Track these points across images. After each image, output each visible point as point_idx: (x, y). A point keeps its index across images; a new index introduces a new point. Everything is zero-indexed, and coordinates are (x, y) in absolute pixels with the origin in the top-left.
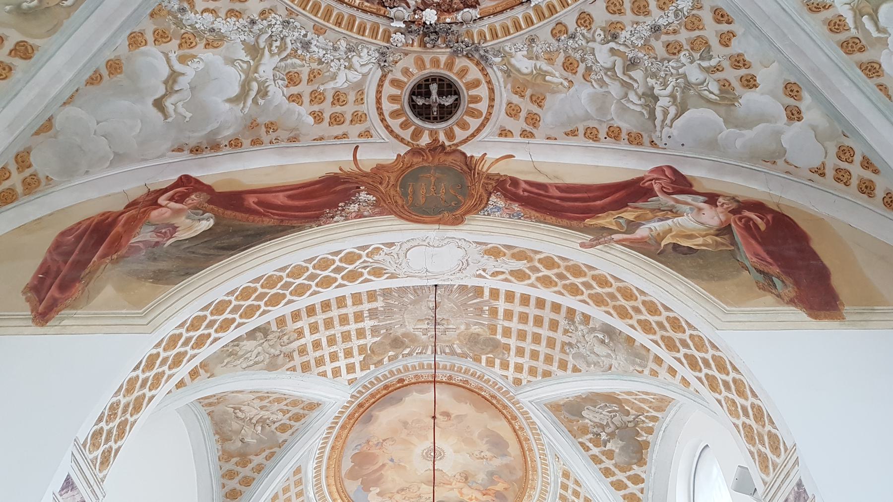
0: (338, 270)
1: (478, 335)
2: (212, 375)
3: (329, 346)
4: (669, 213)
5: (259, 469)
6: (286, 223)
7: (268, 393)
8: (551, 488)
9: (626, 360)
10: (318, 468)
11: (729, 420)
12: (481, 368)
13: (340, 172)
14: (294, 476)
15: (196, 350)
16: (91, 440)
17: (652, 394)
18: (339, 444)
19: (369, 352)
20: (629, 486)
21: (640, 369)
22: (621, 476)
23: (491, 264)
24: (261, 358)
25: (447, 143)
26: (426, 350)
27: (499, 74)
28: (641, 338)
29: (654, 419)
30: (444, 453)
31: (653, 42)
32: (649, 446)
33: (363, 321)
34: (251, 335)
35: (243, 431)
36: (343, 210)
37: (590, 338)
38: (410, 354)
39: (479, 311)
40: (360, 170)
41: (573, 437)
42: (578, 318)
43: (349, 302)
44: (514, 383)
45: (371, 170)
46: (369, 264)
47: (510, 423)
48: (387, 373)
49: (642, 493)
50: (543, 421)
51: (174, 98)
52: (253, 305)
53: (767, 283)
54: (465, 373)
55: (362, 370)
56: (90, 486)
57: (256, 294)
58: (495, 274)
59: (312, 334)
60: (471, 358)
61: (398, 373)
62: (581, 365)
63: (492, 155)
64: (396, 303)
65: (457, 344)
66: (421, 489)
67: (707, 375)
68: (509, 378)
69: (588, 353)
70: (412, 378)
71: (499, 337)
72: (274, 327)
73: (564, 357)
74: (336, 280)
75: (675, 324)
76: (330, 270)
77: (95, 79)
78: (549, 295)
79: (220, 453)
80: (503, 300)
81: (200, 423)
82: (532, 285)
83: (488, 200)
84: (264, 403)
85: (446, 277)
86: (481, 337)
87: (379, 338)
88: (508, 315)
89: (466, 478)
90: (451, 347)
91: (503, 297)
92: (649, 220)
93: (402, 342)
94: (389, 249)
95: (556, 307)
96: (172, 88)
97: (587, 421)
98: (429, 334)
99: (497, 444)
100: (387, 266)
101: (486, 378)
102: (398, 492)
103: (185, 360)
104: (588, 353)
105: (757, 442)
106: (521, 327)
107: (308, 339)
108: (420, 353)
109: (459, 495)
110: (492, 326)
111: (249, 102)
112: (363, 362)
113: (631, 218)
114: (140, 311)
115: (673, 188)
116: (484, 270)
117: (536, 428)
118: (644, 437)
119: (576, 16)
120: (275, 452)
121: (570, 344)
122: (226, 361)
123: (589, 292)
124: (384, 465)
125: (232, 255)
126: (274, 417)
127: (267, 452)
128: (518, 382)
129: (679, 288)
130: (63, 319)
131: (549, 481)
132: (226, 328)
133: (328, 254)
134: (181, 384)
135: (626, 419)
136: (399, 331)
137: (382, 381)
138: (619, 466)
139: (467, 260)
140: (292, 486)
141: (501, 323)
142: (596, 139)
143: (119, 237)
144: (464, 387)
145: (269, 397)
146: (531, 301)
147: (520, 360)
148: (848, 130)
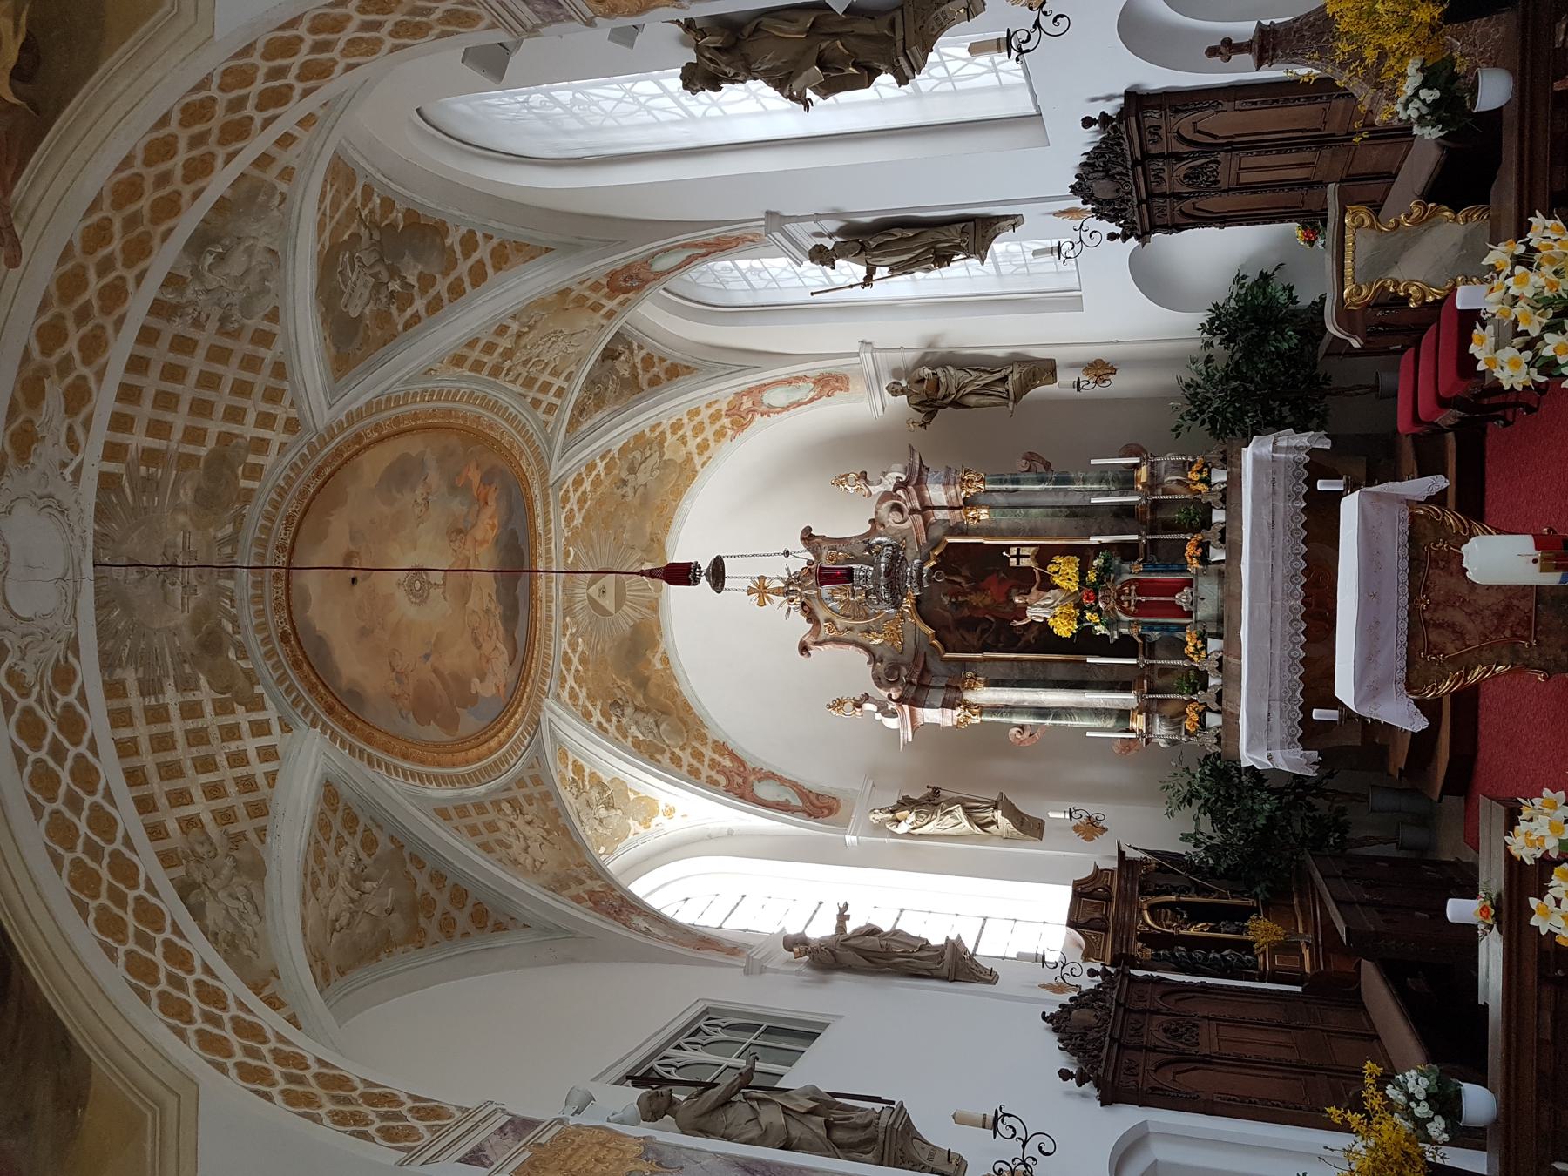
0: (58, 753)
1: (198, 490)
3: (217, 768)
5: (438, 878)
7: (305, 875)
8: (480, 389)
9: (258, 220)
10: (439, 781)
11: (381, 60)
12: (263, 490)
14: (451, 819)
15: (229, 1002)
16: (398, 1141)
17: (324, 186)
19: (228, 695)
20: (479, 257)
21: (278, 198)
22: (463, 268)
23: (50, 451)
26: (228, 589)
28: (219, 184)
29: (368, 192)
33: (165, 707)
34: (197, 912)
35: (372, 912)
37: (212, 281)
38: (234, 621)
39: (148, 485)
41: (395, 341)
42: (171, 297)
43: (125, 733)
44: (294, 432)
46: (45, 692)
47: (368, 447)
48: (269, 664)
49: (491, 238)
50: (363, 390)
52: (135, 911)
54: (272, 521)
55: (263, 708)
56: (476, 1125)
57: (112, 906)
58: (73, 445)
59: (192, 801)
60: (243, 507)
62: (266, 304)
64: (128, 642)
65: (216, 531)
67: (300, 78)
68: (284, 441)
69: (242, 288)
71: (203, 452)
72: (179, 872)
73: (248, 334)
74: (80, 758)
75: (195, 112)
76: (58, 769)
78: (122, 347)
79: (410, 946)
81: (359, 988)
82: (100, 375)
84: (324, 880)
87: (201, 676)
88: (158, 429)
89: (458, 532)
90: (222, 543)
93: (209, 634)
94: (11, 654)
95: (147, 336)
97: (367, 311)
98: (195, 583)
99: (402, 475)
102: (480, 648)
103: (248, 1018)
104: (242, 288)
105: (424, 19)
106: (184, 407)
107: (201, 808)
108: (231, 600)
109: (486, 546)
110: (181, 462)
112: (248, 707)
114: (149, 1116)
116: (64, 465)
117: (377, 403)
118: (398, 216)
121: (223, 320)
122: (246, 952)
123: (119, 264)
124: (435, 671)
125: (22, 964)
126: (350, 862)
127: (410, 867)
129: (119, 89)
131: (468, 391)
132: (184, 955)
133: (21, 773)
134: (293, 1020)
135: (365, 242)
136: (188, 639)
137: (286, 671)
140: (467, 821)
141: (174, 443)
144: (300, 524)
145: (313, 873)
147: (251, 417)
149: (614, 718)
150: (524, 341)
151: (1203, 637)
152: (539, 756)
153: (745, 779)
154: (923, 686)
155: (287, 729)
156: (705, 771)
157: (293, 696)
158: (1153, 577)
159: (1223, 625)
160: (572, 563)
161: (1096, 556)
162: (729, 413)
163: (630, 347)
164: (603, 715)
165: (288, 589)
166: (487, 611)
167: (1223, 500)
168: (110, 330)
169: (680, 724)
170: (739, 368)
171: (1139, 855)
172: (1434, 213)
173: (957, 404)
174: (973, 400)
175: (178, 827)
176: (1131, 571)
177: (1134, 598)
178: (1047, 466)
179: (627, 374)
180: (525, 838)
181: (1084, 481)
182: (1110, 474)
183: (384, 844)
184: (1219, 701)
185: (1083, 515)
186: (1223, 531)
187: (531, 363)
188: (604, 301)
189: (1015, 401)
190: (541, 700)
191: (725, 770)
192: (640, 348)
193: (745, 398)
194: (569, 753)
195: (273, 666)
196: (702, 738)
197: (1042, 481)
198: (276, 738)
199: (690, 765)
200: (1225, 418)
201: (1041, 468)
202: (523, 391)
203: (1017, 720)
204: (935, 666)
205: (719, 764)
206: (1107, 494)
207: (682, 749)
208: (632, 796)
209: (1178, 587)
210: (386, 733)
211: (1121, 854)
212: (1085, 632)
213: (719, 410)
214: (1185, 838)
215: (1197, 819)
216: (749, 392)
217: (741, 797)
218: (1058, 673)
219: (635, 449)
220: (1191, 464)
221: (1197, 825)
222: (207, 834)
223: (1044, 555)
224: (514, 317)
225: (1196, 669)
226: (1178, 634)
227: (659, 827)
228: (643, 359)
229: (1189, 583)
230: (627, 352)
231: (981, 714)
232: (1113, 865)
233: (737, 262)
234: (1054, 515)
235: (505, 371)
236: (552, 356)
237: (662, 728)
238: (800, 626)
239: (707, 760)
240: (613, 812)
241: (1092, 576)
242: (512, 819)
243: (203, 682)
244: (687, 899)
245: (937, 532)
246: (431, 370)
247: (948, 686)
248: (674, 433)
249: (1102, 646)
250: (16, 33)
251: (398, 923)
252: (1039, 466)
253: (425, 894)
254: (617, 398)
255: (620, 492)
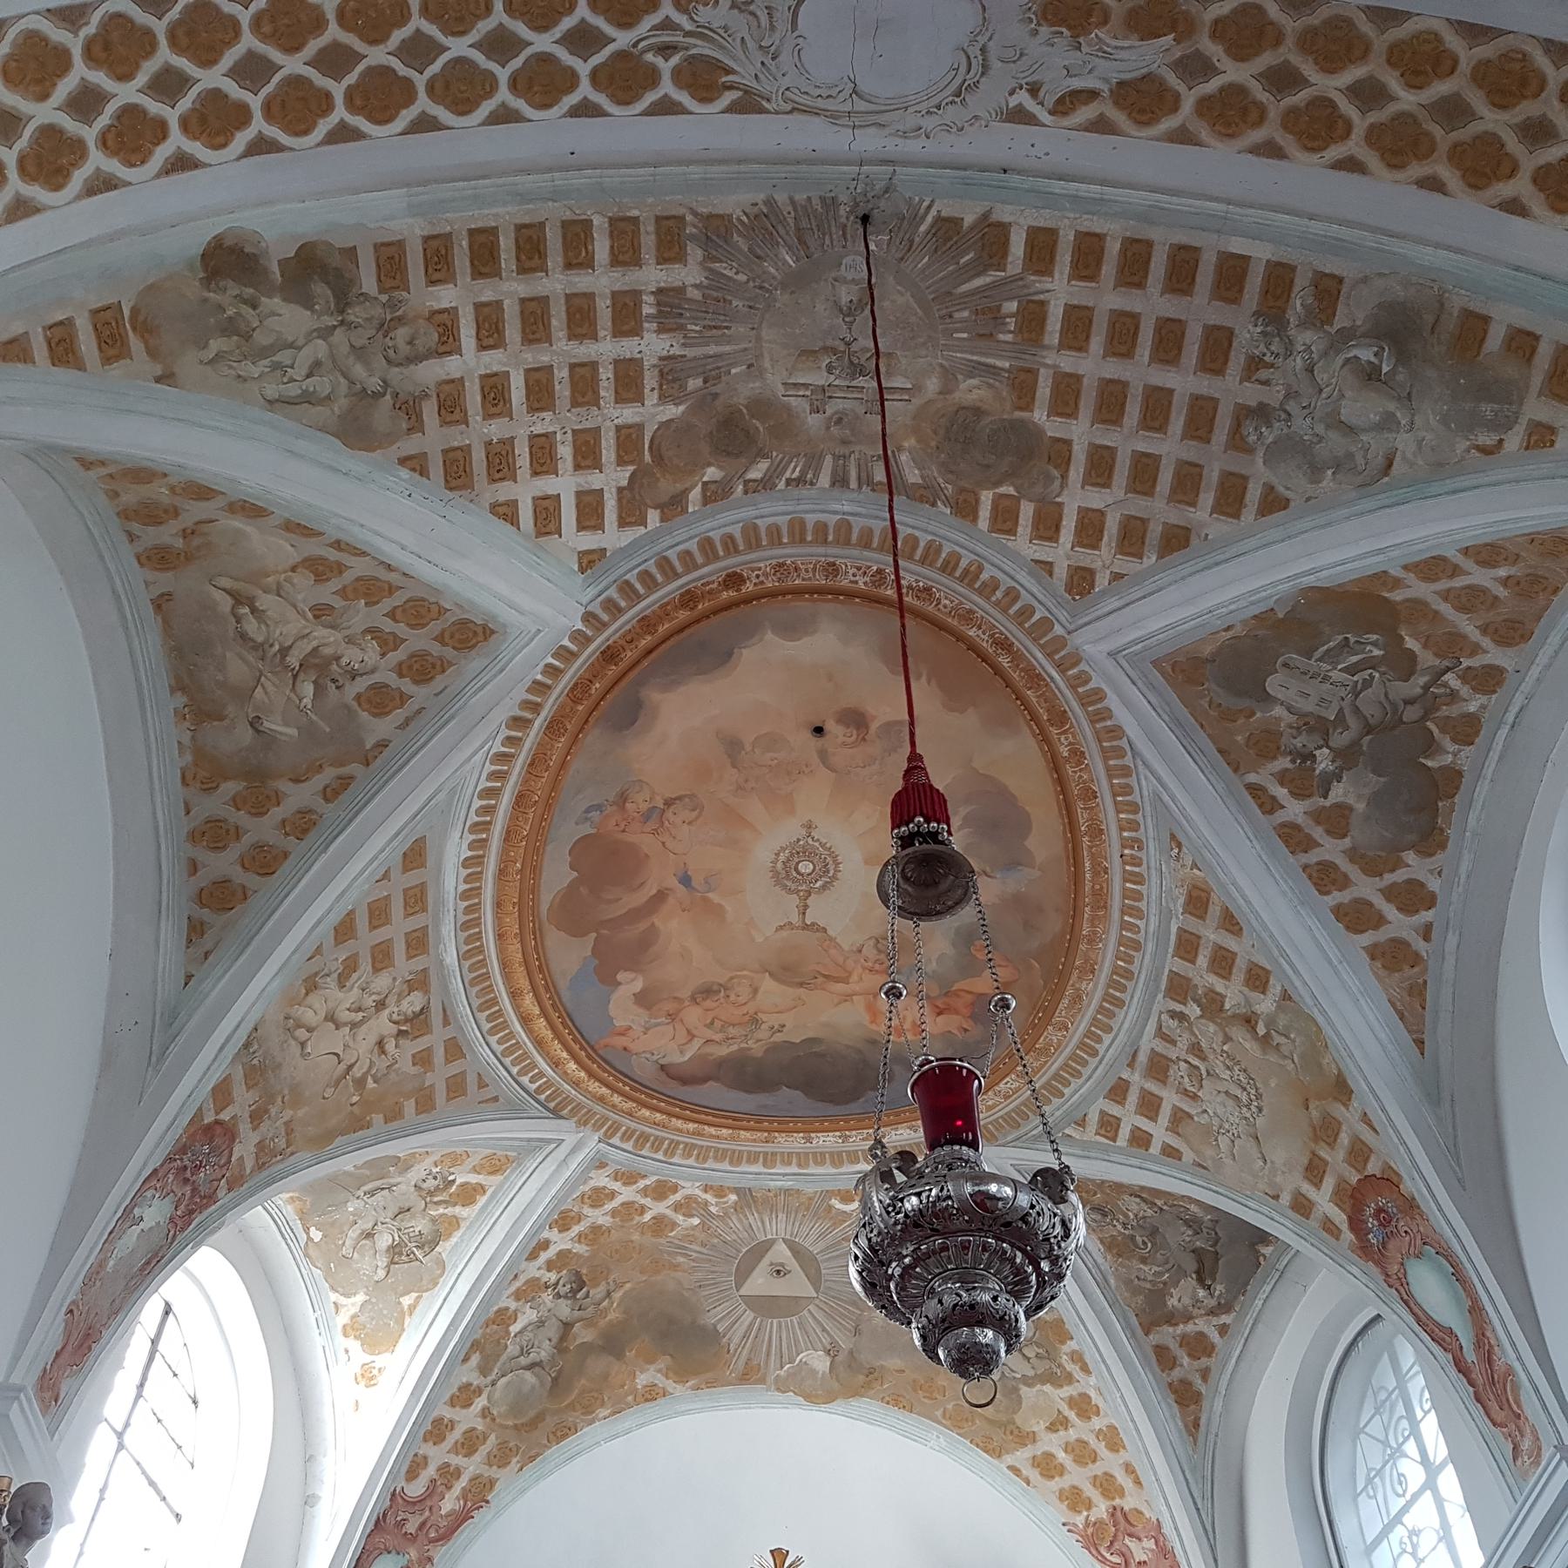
1: (978, 412)
2: (166, 378)
3: (532, 410)
5: (303, 825)
8: (1143, 964)
14: (406, 870)
18: (541, 785)
19: (647, 458)
20: (1390, 918)
22: (1366, 888)
24: (321, 385)
30: (837, 864)
32: (1458, 788)
33: (636, 332)
35: (259, 689)
38: (766, 484)
41: (1229, 770)
46: (678, 38)
49: (1427, 938)
55: (623, 523)
58: (1066, 104)
59: (482, 347)
61: (728, 553)
62: (1290, 481)
64: (742, 278)
66: (759, 996)
68: (1056, 570)
69: (1320, 429)
70: (766, 575)
71: (1039, 415)
79: (189, 758)
80: (1067, 270)
85: (911, 120)
86: (986, 420)
87: (681, 408)
88: (1078, 325)
91: (1068, 258)
97: (1278, 711)
98: (829, 412)
100: (733, 58)
101: (984, 576)
102: (693, 999)
104: (1320, 429)
116: (1034, 90)
118: (1449, 754)
120: (352, 778)
121: (1262, 413)
124: (661, 896)
126: (351, 656)
127: (328, 775)
128: (1081, 582)
131: (1140, 937)
138: (1363, 856)
139: (983, 50)
146: (1152, 265)
147: (1096, 499)
149: (552, 1277)
150: (1239, 1033)
152: (495, 1104)
153: (412, 1538)
155: (585, 561)
156: (438, 1455)
157: (638, 586)
160: (830, 1207)
162: (1118, 1513)
163: (1223, 1307)
164: (562, 1255)
165: (813, 591)
166: (755, 1021)
168: (1257, 136)
169: (532, 1413)
170: (1209, 1529)
175: (443, 306)
179: (1172, 1302)
180: (354, 1025)
183: (378, 728)
187: (1196, 1062)
188: (1329, 1183)
190: (597, 1128)
191: (436, 1498)
192: (1223, 1330)
193: (1151, 1544)
194: (498, 1178)
195: (688, 553)
196: (501, 1458)
198: (572, 539)
199: (452, 1425)
202: (1142, 1058)
205: (449, 1487)
207: (485, 1412)
208: (407, 1301)
210: (563, 765)
213: (1121, 1492)
217: (379, 1524)
222: (426, 357)
224: (1286, 996)
227: (342, 1355)
228: (1201, 1334)
230: (1213, 1302)
233: (1450, 1467)
235: (1178, 1007)
236: (1214, 1105)
237: (528, 1375)
239: (456, 1460)
240: (382, 1261)
242: (392, 1008)
243: (673, 411)
244: (195, 1402)
246: (1179, 846)
248: (1072, 1402)
251: (234, 738)
253: (278, 799)
254: (1128, 1283)
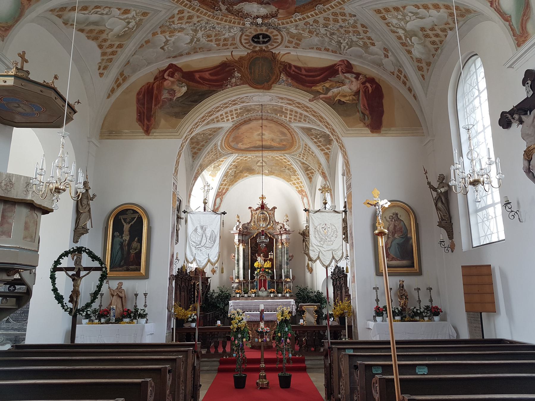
4: (341, 84)
5: (203, 146)
6: (212, 89)
13: (227, 60)
22: (323, 148)
25: (266, 49)
27: (285, 33)
31: (340, 29)
36: (230, 82)
40: (234, 59)
45: (238, 59)
51: (167, 46)
53: (363, 120)
63: (282, 52)
77: (142, 46)
83: (280, 76)
92: (333, 88)
96: (166, 44)
111: (193, 43)
113: (328, 86)
115: (346, 69)
119: (313, 20)
129: (336, 120)
130: (153, 133)
142: (320, 50)
143: (157, 97)
148: (401, 66)
151: (255, 293)
152: (224, 155)
154: (243, 235)
156: (222, 187)
158: (267, 283)
159: (257, 297)
161: (271, 271)
167: (283, 296)
171: (209, 281)
172: (316, 318)
173: (304, 240)
174: (304, 244)
176: (268, 278)
177: (263, 279)
178: (291, 260)
179: (309, 169)
181: (287, 268)
182: (288, 273)
183: (210, 137)
184: (242, 296)
185: (281, 267)
186: (277, 296)
189: (304, 253)
196: (229, 185)
197: (287, 259)
199: (223, 184)
200: (299, 295)
201: (290, 259)
203: (236, 255)
204: (247, 237)
206: (284, 273)
207: (227, 181)
208: (216, 172)
209: (265, 288)
211: (209, 278)
212: (255, 269)
214: (213, 290)
215: (217, 293)
216: (306, 195)
217: (217, 195)
218: (246, 263)
219: (293, 170)
220: (290, 289)
221: (216, 293)
223: (271, 260)
224: (315, 155)
225: (248, 292)
226: (255, 288)
229: (266, 290)
231: (237, 248)
232: (207, 276)
234: (280, 262)
238: (255, 207)
241: (267, 270)
245: (276, 237)
247: (243, 240)
248: (297, 178)
249: (252, 273)
250: (346, 100)
252: (290, 258)
255: (284, 167)
